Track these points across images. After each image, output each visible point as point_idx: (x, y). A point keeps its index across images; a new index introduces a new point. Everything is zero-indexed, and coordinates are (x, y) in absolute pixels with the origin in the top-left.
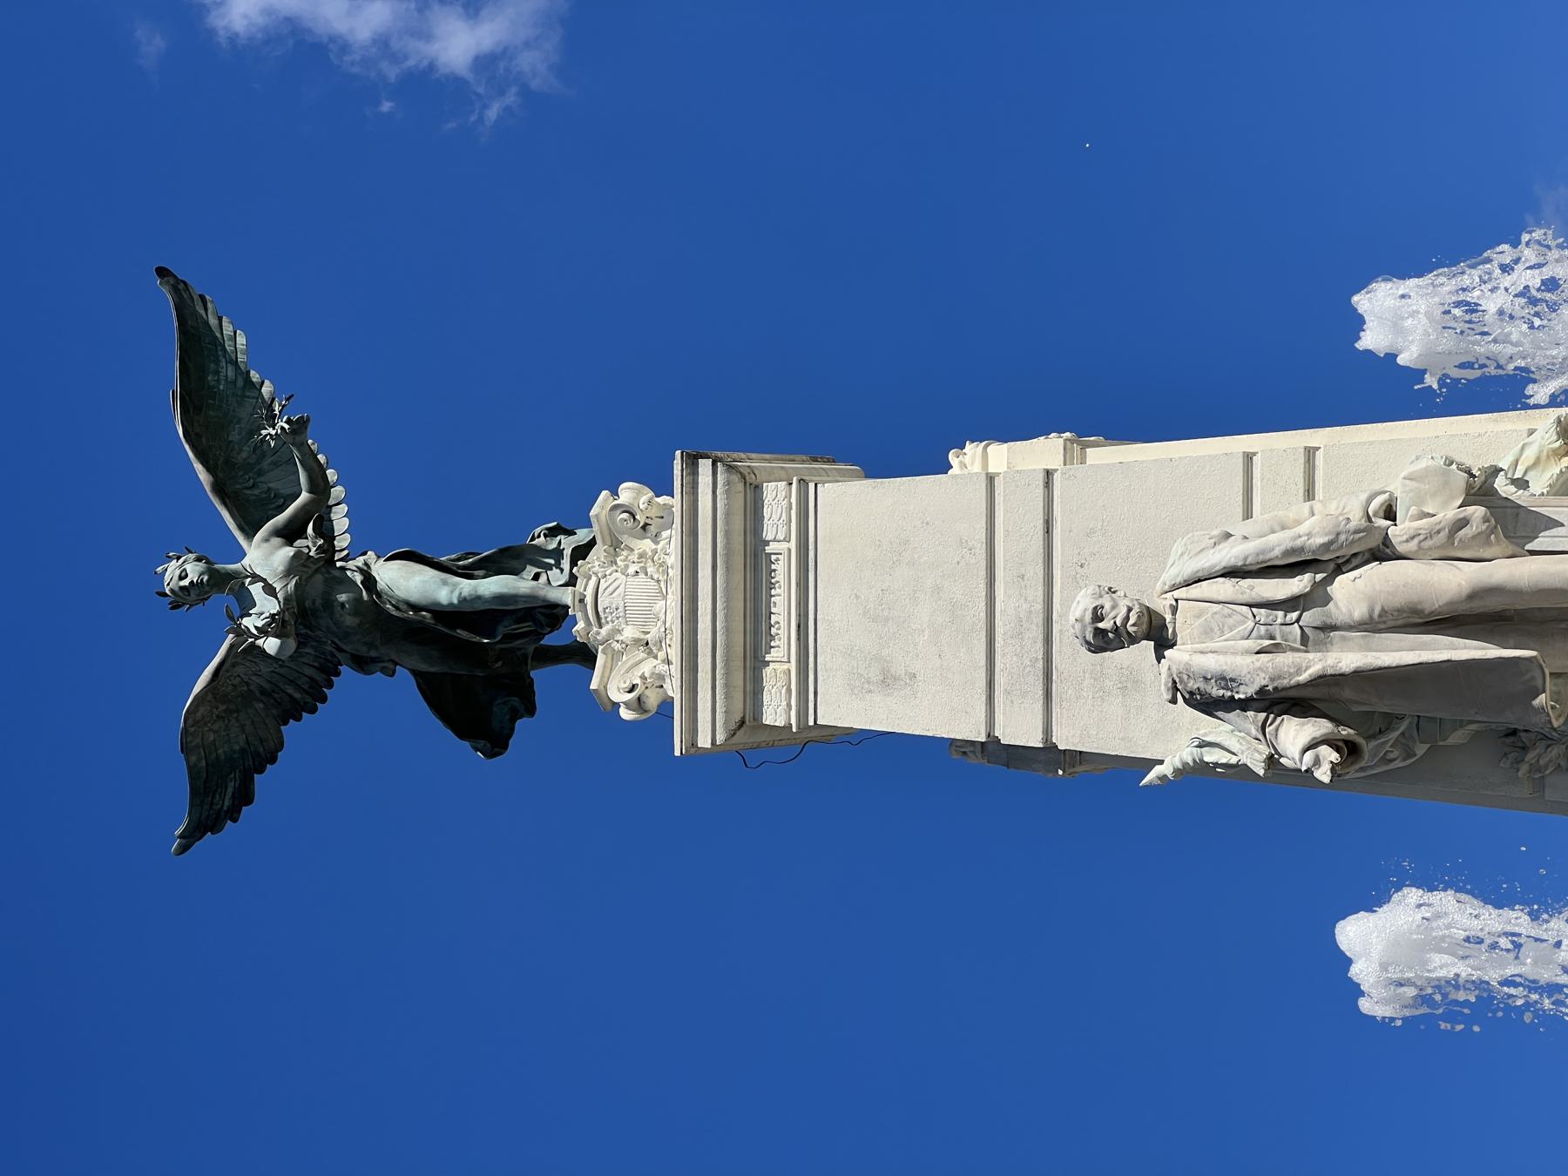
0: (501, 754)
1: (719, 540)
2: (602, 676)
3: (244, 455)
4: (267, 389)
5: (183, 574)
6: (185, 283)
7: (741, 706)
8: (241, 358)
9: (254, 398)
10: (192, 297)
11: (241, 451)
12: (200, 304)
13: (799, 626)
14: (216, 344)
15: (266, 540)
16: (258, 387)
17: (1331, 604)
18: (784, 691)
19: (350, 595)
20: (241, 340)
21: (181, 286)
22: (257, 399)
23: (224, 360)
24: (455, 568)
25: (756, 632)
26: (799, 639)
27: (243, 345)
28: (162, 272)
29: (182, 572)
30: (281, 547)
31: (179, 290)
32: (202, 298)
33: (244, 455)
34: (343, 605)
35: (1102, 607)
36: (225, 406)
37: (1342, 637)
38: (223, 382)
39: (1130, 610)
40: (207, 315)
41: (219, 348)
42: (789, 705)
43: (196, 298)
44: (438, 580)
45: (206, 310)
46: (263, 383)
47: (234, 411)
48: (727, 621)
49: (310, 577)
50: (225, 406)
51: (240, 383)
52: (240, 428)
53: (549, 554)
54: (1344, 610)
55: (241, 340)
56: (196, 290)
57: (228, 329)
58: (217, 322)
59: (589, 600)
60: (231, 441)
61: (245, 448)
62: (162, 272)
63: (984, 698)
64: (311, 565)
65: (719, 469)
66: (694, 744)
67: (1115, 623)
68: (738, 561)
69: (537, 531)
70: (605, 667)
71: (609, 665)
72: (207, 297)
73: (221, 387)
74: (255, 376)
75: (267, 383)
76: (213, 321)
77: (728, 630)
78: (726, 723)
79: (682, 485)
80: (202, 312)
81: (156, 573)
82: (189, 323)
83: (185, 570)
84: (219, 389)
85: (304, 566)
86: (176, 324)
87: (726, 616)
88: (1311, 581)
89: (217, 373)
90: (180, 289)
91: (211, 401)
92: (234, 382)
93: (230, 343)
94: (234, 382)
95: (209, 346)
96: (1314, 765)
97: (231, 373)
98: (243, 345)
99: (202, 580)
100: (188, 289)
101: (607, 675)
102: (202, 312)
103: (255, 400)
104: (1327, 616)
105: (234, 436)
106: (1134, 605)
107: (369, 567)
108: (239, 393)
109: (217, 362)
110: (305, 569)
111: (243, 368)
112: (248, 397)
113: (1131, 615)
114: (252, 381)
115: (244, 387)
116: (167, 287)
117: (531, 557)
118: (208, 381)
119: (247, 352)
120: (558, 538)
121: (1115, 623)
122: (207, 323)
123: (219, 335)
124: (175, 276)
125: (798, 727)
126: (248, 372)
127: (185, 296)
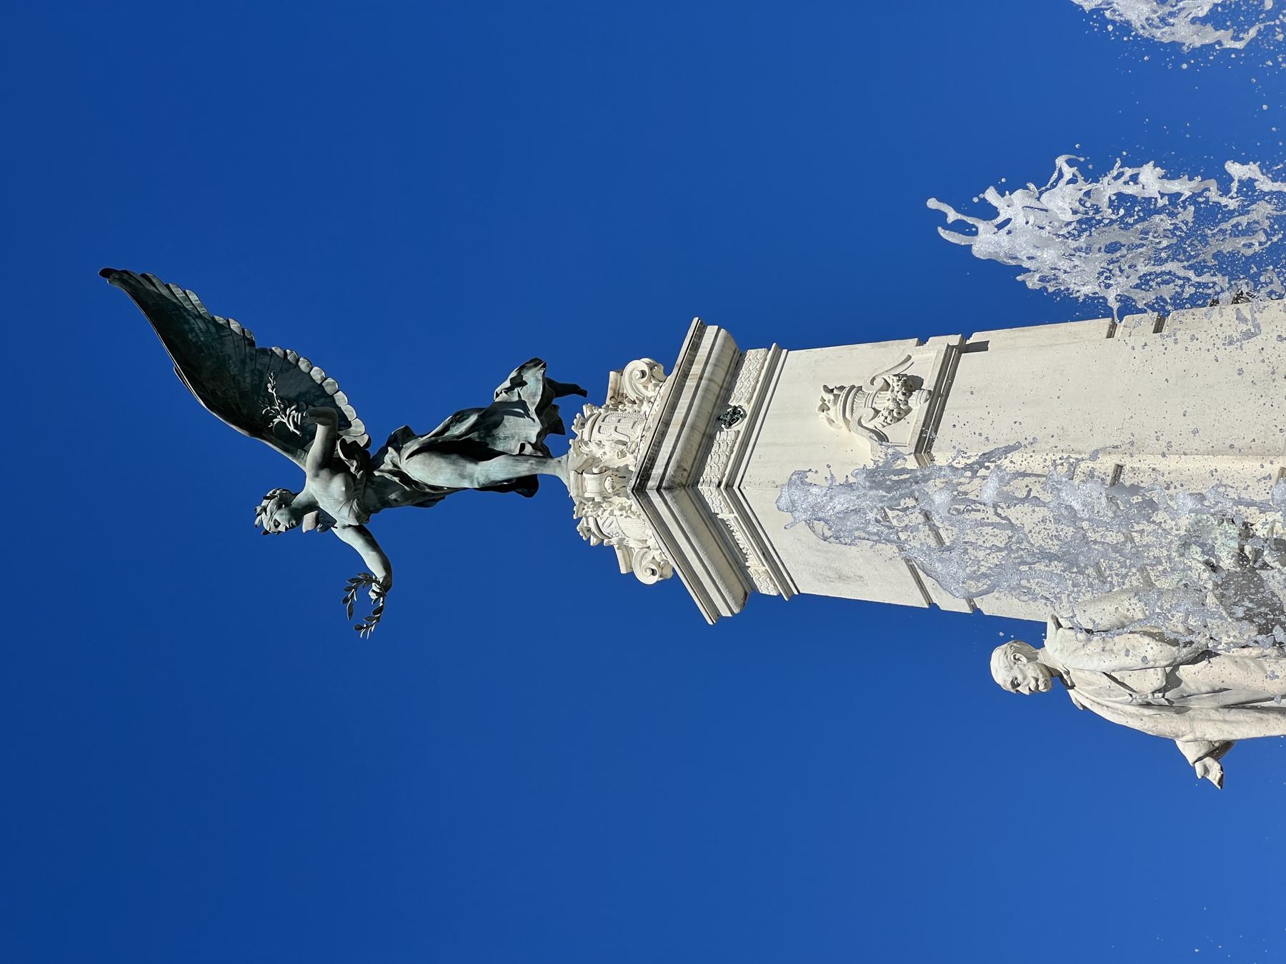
0: (535, 492)
1: (684, 526)
2: (626, 563)
3: (248, 380)
4: (234, 326)
5: (277, 524)
6: (125, 272)
7: (741, 588)
8: (202, 311)
9: (228, 335)
10: (137, 280)
11: (245, 378)
12: (147, 283)
13: (763, 554)
14: (178, 308)
15: (317, 476)
16: (227, 326)
17: (1183, 685)
18: (768, 580)
19: (397, 493)
20: (193, 297)
21: (126, 276)
22: (231, 334)
23: (191, 318)
24: (456, 439)
25: (732, 552)
26: (766, 560)
27: (197, 301)
28: (106, 273)
29: (274, 523)
30: (331, 479)
31: (125, 280)
32: (144, 276)
33: (248, 380)
34: (395, 500)
35: (1016, 679)
36: (213, 352)
37: (1197, 699)
38: (201, 335)
39: (1037, 680)
40: (157, 288)
41: (182, 310)
42: (775, 585)
43: (141, 279)
44: (457, 476)
45: (154, 285)
46: (228, 322)
47: (222, 352)
48: (715, 566)
49: (364, 492)
50: (213, 352)
51: (213, 329)
52: (233, 362)
53: (516, 404)
54: (1193, 687)
55: (193, 297)
56: (137, 273)
57: (179, 293)
58: (167, 291)
59: (594, 529)
60: (234, 375)
61: (246, 375)
62: (106, 273)
63: (918, 590)
64: (360, 486)
65: (664, 493)
66: (719, 615)
67: (1030, 689)
68: (702, 527)
69: (498, 390)
70: (624, 557)
71: (626, 554)
72: (149, 275)
73: (202, 339)
74: (220, 320)
75: (231, 321)
76: (164, 292)
77: (713, 563)
78: (736, 603)
79: (641, 506)
80: (152, 288)
81: (256, 526)
82: (150, 303)
83: (276, 520)
84: (202, 341)
85: (355, 490)
86: (143, 312)
87: (709, 558)
88: (1163, 675)
89: (192, 330)
90: (123, 278)
91: (203, 354)
92: (208, 330)
93: (187, 303)
94: (208, 330)
95: (174, 312)
96: (1205, 773)
97: (202, 325)
98: (197, 301)
99: (292, 524)
100: (132, 276)
101: (628, 560)
102: (152, 288)
103: (231, 337)
104: (1183, 692)
105: (234, 370)
106: (1038, 675)
107: (398, 467)
108: (217, 337)
109: (187, 322)
110: (358, 492)
111: (208, 318)
112: (224, 336)
113: (1039, 683)
114: (220, 324)
115: (217, 330)
116: (116, 283)
117: (504, 410)
118: (191, 340)
119: (203, 304)
120: (516, 390)
121: (1030, 689)
122: (161, 295)
123: (175, 301)
124: (115, 271)
125: (788, 597)
126: (213, 318)
127: (133, 283)
